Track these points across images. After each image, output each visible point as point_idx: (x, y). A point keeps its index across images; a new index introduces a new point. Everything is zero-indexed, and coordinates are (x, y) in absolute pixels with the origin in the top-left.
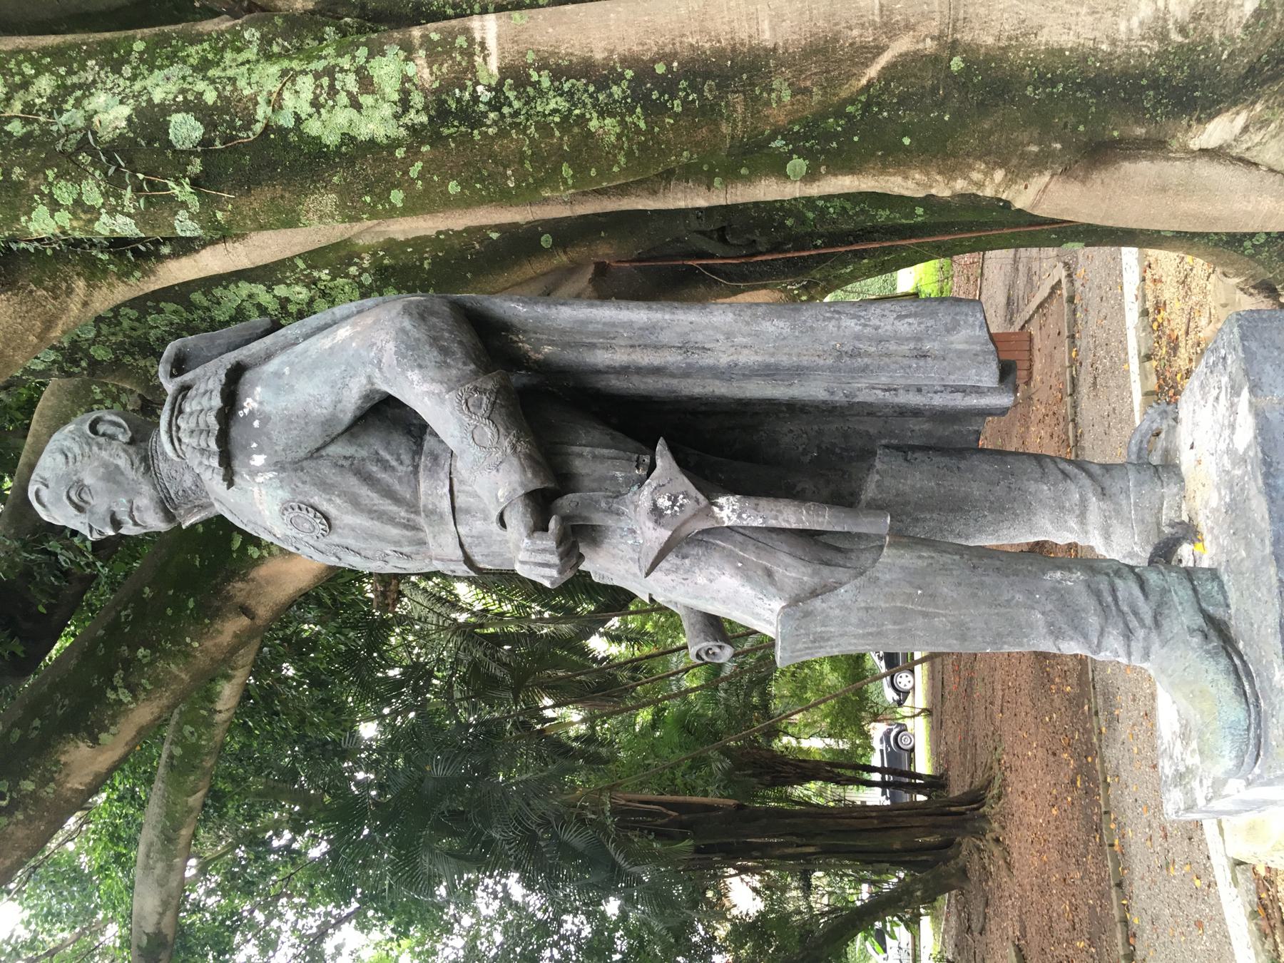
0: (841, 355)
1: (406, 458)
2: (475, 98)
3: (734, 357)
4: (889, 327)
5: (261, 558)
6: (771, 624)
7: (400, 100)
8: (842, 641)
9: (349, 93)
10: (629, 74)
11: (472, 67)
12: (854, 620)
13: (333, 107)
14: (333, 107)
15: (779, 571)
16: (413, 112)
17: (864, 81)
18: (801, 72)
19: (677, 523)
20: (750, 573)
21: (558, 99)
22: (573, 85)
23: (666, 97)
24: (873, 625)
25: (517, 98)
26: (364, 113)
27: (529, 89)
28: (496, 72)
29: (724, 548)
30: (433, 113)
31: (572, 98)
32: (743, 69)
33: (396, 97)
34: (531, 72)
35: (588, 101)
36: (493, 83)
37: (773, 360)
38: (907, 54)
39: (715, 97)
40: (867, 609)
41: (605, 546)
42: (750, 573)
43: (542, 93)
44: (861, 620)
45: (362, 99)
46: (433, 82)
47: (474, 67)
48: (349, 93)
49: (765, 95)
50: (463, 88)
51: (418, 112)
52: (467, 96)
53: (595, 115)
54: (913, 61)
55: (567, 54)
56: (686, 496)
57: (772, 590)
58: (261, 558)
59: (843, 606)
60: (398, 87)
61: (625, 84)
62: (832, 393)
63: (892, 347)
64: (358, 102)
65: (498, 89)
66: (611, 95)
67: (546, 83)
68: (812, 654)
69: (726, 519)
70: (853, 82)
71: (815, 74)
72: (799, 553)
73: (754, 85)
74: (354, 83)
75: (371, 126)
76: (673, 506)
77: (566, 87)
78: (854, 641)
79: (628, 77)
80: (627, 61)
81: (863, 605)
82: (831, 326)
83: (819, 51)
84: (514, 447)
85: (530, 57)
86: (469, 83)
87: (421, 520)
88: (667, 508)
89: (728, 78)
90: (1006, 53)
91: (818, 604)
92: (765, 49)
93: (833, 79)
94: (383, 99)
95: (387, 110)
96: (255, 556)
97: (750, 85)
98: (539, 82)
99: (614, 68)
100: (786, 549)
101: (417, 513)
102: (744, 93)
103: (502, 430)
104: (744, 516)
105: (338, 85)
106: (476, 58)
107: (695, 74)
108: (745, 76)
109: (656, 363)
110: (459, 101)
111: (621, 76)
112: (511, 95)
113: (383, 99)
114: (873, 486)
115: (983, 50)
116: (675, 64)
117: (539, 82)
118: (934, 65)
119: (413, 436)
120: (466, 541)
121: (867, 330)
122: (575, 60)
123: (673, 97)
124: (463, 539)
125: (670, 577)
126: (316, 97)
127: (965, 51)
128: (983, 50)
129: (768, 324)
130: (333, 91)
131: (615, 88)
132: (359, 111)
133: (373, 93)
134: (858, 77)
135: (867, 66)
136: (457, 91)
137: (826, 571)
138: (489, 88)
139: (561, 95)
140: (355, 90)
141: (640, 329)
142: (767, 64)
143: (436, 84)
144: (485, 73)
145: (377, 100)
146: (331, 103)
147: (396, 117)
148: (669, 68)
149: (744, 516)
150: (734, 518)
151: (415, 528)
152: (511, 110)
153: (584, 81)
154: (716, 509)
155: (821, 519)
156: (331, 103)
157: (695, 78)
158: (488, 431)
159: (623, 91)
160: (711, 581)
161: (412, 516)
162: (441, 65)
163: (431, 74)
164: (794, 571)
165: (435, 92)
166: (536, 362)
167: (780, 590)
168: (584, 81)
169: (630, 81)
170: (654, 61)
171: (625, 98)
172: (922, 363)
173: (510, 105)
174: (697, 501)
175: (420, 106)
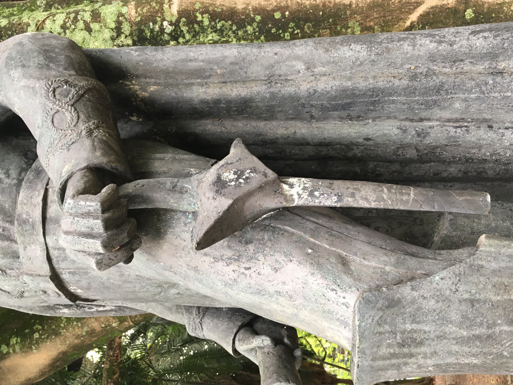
0: (414, 77)
1: (14, 173)
2: (162, 30)
3: (314, 84)
4: (465, 42)
5: (8, 353)
6: (345, 324)
7: (116, 28)
8: (441, 346)
9: (85, 22)
10: (258, 18)
11: (161, 10)
12: (455, 316)
13: (74, 29)
14: (74, 29)
15: (356, 261)
16: (123, 36)
17: (408, 23)
18: (367, 17)
19: (240, 192)
20: (321, 261)
21: (214, 34)
22: (223, 25)
23: (281, 31)
24: (481, 324)
25: (188, 32)
26: (93, 35)
27: (196, 26)
28: (176, 13)
29: (293, 234)
30: (135, 38)
31: (222, 34)
32: (330, 17)
33: (113, 25)
34: (198, 14)
35: (232, 35)
36: (174, 20)
37: (349, 84)
38: (436, 7)
39: (311, 31)
40: (472, 302)
41: (169, 236)
42: (321, 261)
43: (203, 30)
44: (465, 317)
45: (92, 26)
46: (137, 17)
47: (163, 9)
48: (85, 22)
49: (344, 30)
50: (155, 23)
51: (126, 37)
52: (157, 28)
53: (235, 40)
54: (440, 12)
55: (221, 5)
56: (254, 170)
57: (348, 280)
58: (8, 353)
59: (440, 296)
60: (115, 19)
61: (255, 25)
62: (405, 131)
63: (467, 67)
64: (89, 27)
65: (176, 24)
66: (246, 31)
67: (206, 22)
68: (398, 367)
69: (296, 197)
70: (401, 23)
71: (376, 18)
72: (379, 243)
73: (337, 25)
74: (89, 16)
75: (97, 44)
76: (237, 179)
77: (219, 26)
78: (455, 348)
79: (257, 20)
80: (257, 10)
81: (466, 296)
82: (406, 47)
83: (379, 6)
84: (90, 132)
85: (197, 6)
86: (159, 19)
87: (15, 230)
88: (231, 181)
89: (320, 22)
90: (502, 8)
91: (406, 291)
92: (344, 5)
93: (388, 21)
94: (105, 26)
95: (107, 34)
96: (5, 352)
97: (334, 25)
98: (202, 21)
99: (249, 15)
100: (362, 237)
101: (12, 222)
102: (330, 29)
103: (82, 116)
104: (317, 193)
105: (79, 17)
106: (165, 5)
107: (299, 19)
108: (331, 20)
109: (243, 94)
110: (152, 31)
111: (253, 20)
112: (185, 29)
113: (105, 26)
114: (447, 225)
115: (486, 5)
116: (287, 13)
117: (202, 21)
118: (454, 14)
119: (27, 158)
120: (54, 254)
121: (443, 47)
122: (225, 8)
123: (284, 32)
124: (51, 252)
125: (232, 267)
126: (65, 23)
127: (474, 6)
128: (486, 5)
129: (346, 48)
130: (75, 20)
131: (249, 27)
132: (90, 33)
133: (100, 22)
134: (404, 20)
135: (410, 14)
136: (151, 24)
137: (413, 262)
138: (171, 24)
139: (215, 32)
140: (89, 20)
141: (232, 63)
142: (345, 13)
143: (139, 19)
144: (169, 14)
145: (101, 27)
146: (73, 27)
147: (113, 39)
148: (283, 15)
149: (317, 193)
150: (305, 195)
151: (10, 239)
152: (184, 40)
153: (230, 22)
154: (285, 187)
155: (405, 198)
156: (73, 27)
157: (299, 21)
158: (68, 115)
159: (254, 29)
160: (276, 270)
161: (7, 225)
162: (143, 8)
163: (136, 12)
164: (374, 259)
165: (138, 24)
166: (143, 100)
167: (358, 279)
168: (230, 22)
169: (258, 23)
170: (274, 11)
171: (255, 33)
172: (499, 79)
173: (184, 37)
174: (265, 175)
175: (127, 33)
